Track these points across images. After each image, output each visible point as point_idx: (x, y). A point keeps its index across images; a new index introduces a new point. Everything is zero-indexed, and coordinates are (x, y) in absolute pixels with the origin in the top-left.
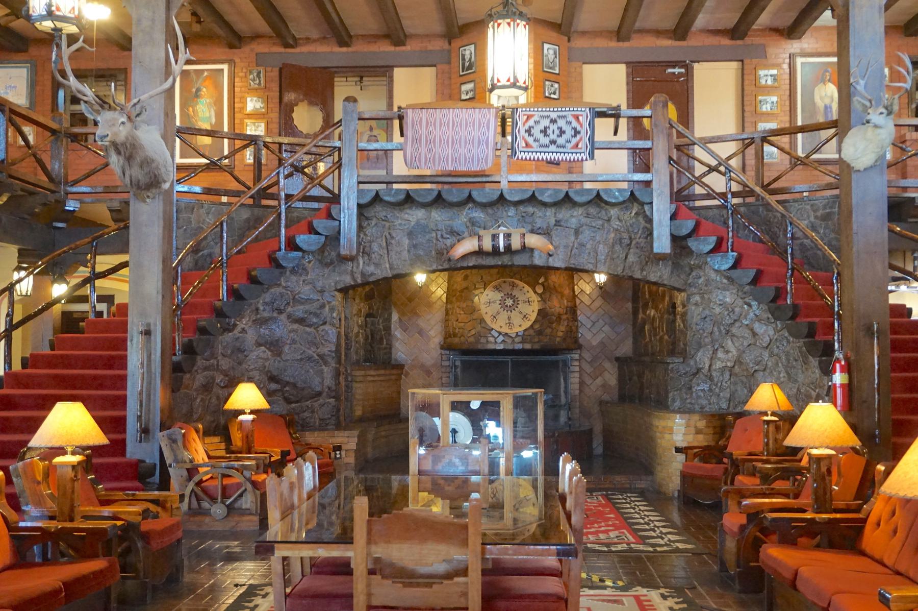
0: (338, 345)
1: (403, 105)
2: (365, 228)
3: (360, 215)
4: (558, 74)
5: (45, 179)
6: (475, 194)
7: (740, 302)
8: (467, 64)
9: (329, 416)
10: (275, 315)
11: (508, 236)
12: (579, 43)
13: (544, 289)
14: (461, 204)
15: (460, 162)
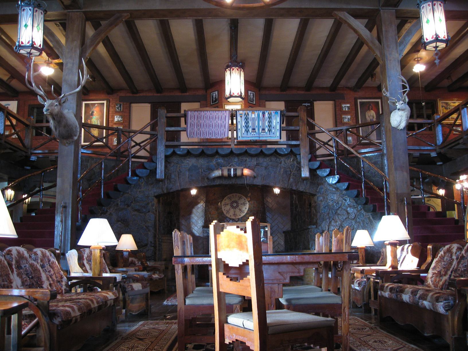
0: (155, 222)
1: (186, 110)
3: (166, 161)
5: (21, 145)
6: (219, 151)
7: (341, 199)
8: (214, 100)
9: (151, 255)
10: (126, 207)
11: (235, 170)
12: (264, 92)
13: (251, 199)
14: (212, 156)
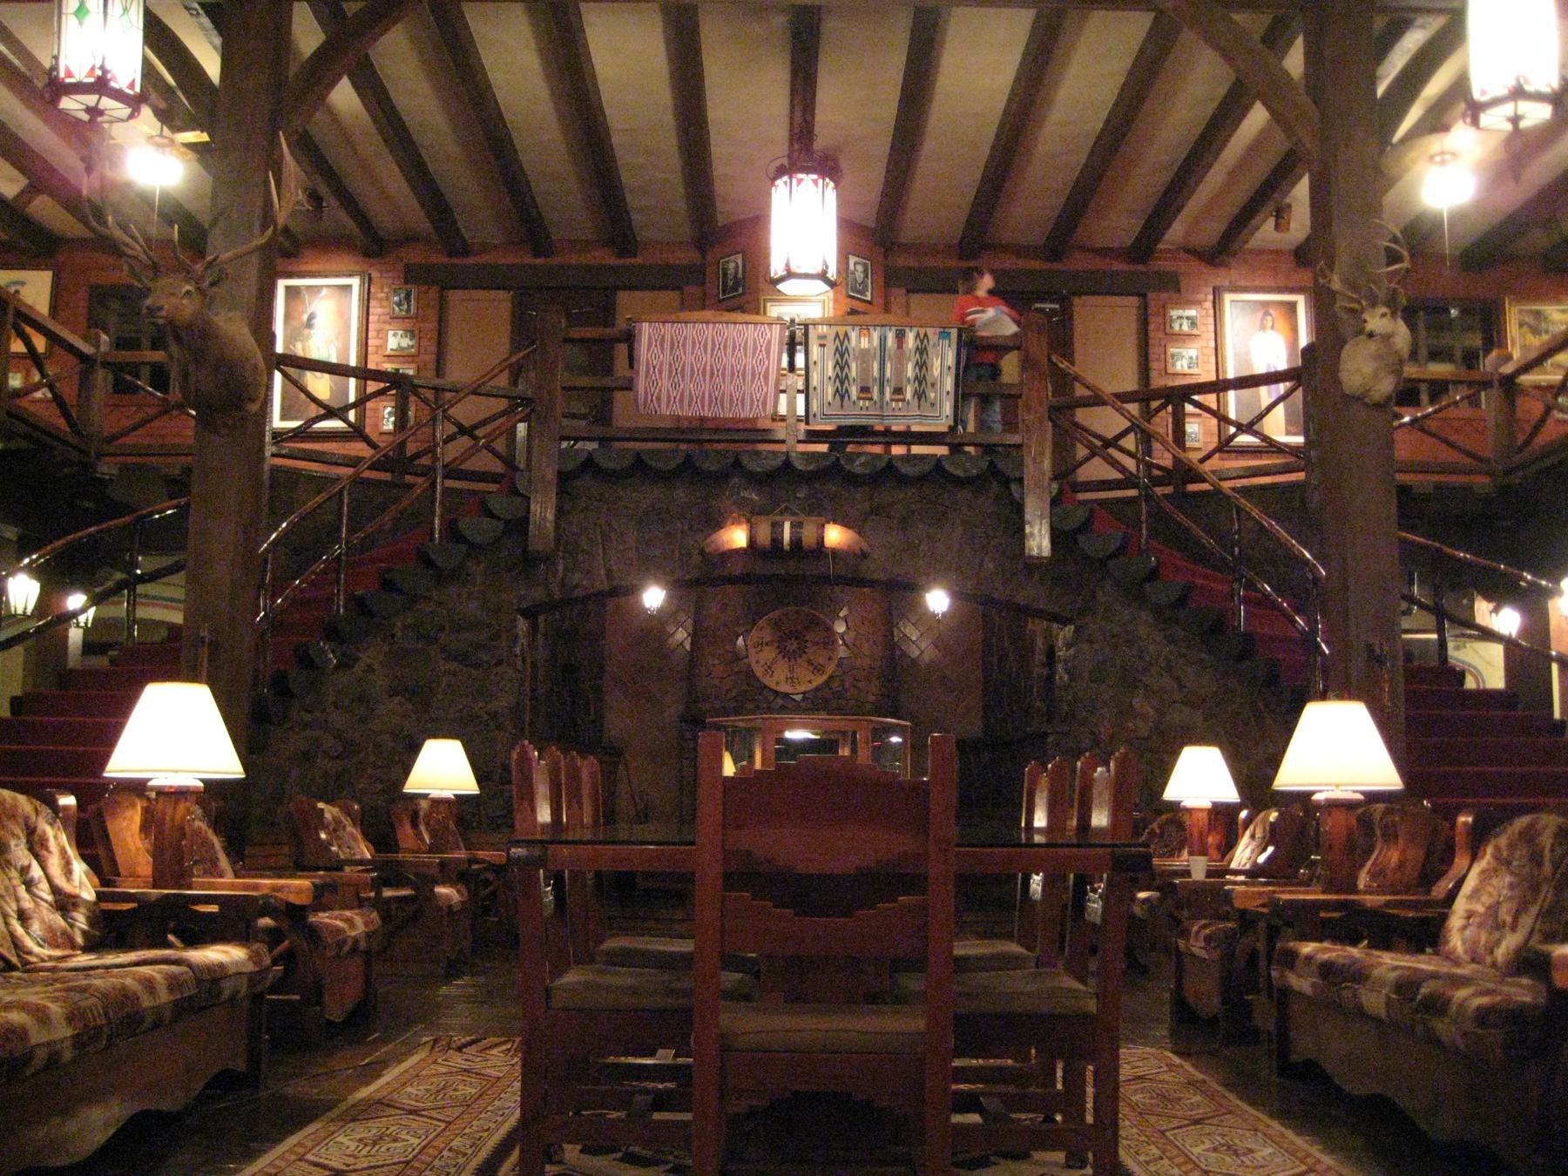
2: (569, 512)
4: (870, 303)
8: (730, 283)
15: (722, 405)
